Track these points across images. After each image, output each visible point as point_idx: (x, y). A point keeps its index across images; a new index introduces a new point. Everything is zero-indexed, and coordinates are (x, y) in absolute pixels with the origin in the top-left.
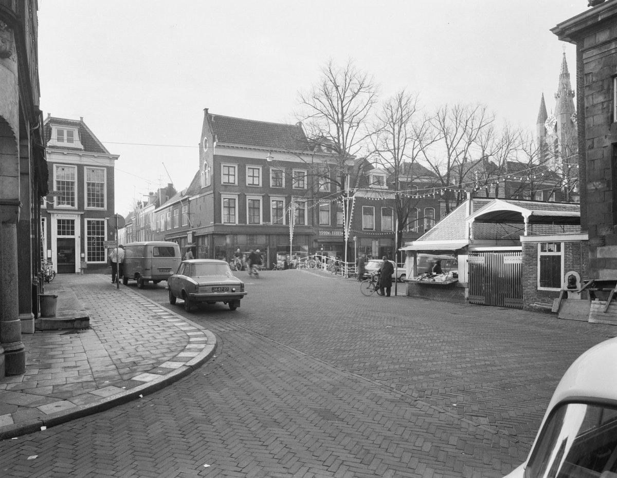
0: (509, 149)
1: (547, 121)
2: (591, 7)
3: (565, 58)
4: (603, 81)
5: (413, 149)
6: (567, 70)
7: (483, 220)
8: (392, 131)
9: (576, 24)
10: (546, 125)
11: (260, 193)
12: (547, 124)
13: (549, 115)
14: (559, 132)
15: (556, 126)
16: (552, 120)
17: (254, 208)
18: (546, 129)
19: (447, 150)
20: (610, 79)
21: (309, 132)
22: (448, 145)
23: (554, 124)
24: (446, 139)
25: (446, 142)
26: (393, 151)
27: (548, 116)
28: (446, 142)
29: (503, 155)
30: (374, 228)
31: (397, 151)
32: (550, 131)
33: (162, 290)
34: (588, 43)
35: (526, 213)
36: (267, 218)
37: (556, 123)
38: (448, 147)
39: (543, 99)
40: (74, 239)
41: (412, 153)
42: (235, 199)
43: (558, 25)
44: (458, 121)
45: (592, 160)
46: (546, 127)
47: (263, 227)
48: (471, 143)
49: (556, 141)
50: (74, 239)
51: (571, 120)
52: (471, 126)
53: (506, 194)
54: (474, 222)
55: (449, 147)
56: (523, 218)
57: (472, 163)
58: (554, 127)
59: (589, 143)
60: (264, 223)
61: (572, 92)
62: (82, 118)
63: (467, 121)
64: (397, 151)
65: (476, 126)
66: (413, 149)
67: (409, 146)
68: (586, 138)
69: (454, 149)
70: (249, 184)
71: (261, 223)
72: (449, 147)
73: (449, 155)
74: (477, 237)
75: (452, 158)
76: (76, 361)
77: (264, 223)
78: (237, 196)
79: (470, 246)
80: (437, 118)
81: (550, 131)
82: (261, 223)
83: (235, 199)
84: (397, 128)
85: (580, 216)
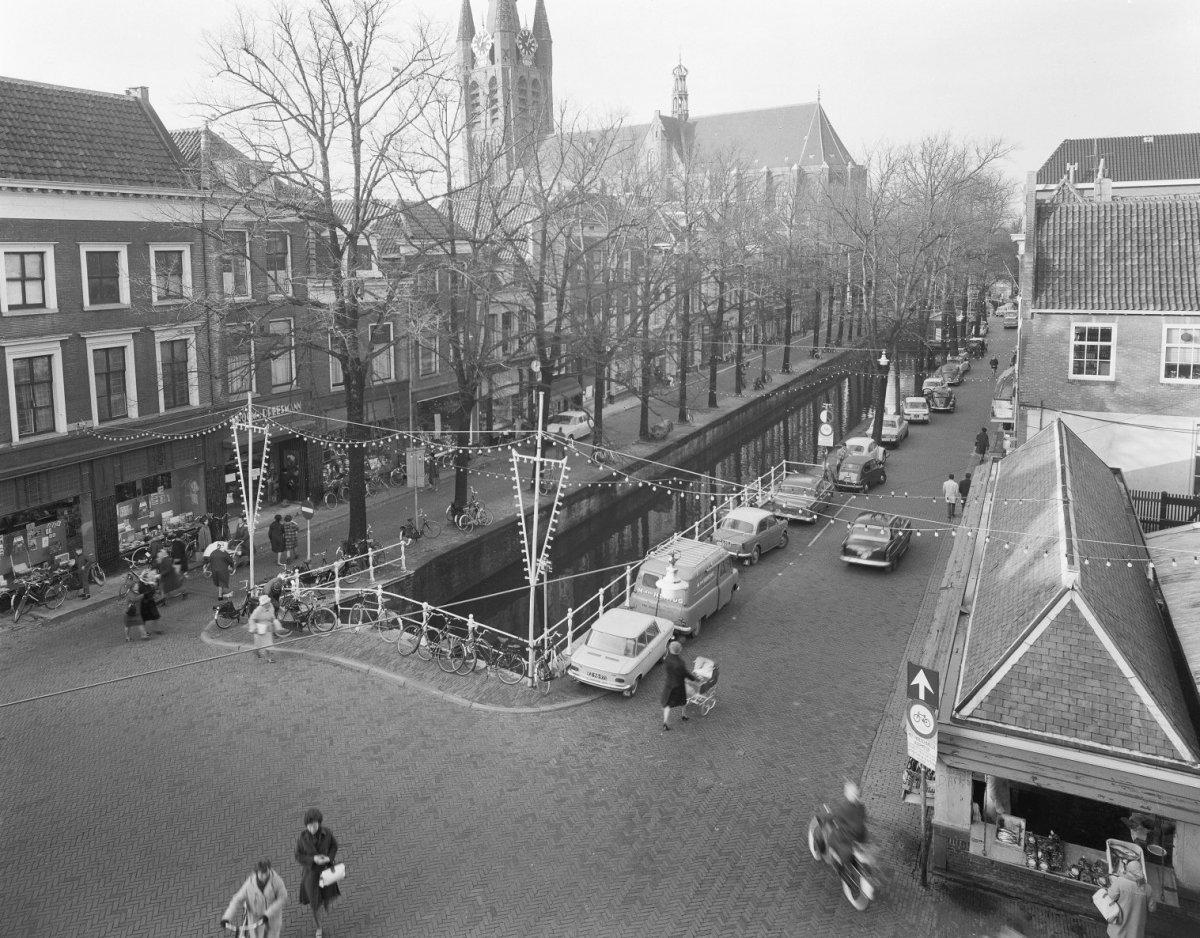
11: (53, 332)
14: (498, 65)
17: (112, 375)
18: (473, 55)
21: (176, 117)
30: (393, 376)
32: (482, 59)
33: (778, 554)
36: (77, 407)
40: (1110, 347)
42: (50, 357)
46: (475, 50)
47: (70, 441)
49: (494, 79)
50: (1110, 347)
57: (677, 130)
60: (73, 427)
62: (144, 90)
70: (11, 307)
71: (62, 427)
76: (1123, 740)
77: (73, 427)
78: (58, 345)
81: (482, 59)
82: (62, 427)
83: (50, 357)
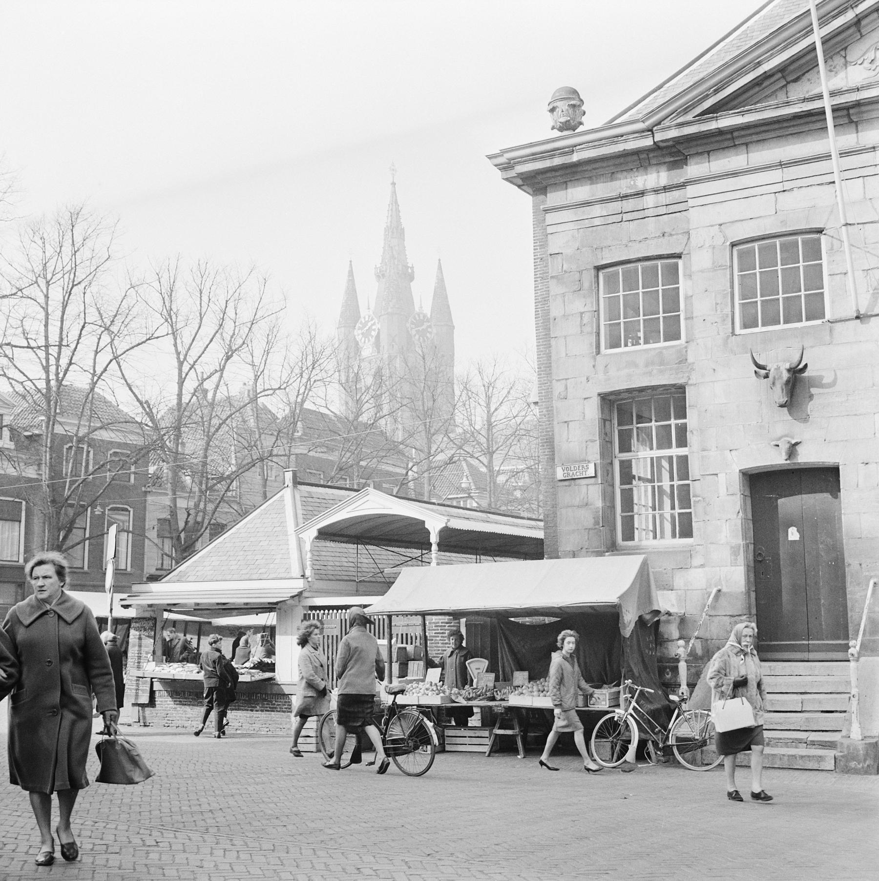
0: (312, 380)
1: (358, 325)
2: (557, 134)
3: (394, 193)
4: (581, 272)
5: (96, 352)
6: (399, 218)
7: (334, 535)
8: (42, 300)
9: (535, 157)
10: (358, 333)
12: (360, 332)
13: (364, 312)
15: (378, 337)
16: (369, 324)
18: (357, 343)
19: (176, 364)
20: (593, 272)
22: (178, 354)
23: (374, 333)
24: (175, 339)
25: (175, 345)
26: (42, 354)
27: (362, 315)
28: (175, 345)
29: (302, 391)
31: (53, 351)
34: (555, 198)
35: (435, 524)
37: (379, 333)
38: (178, 358)
39: (351, 273)
41: (91, 363)
43: (504, 152)
44: (205, 299)
45: (566, 422)
46: (358, 338)
48: (232, 355)
51: (408, 331)
52: (233, 316)
53: (145, 500)
54: (317, 538)
55: (182, 357)
56: (429, 533)
58: (373, 340)
59: (558, 388)
61: (410, 271)
63: (227, 301)
64: (53, 351)
65: (245, 315)
66: (96, 352)
67: (89, 342)
68: (555, 377)
69: (192, 367)
72: (182, 357)
73: (181, 383)
74: (321, 575)
75: (190, 384)
79: (305, 594)
80: (156, 284)
84: (56, 294)
85: (543, 537)
